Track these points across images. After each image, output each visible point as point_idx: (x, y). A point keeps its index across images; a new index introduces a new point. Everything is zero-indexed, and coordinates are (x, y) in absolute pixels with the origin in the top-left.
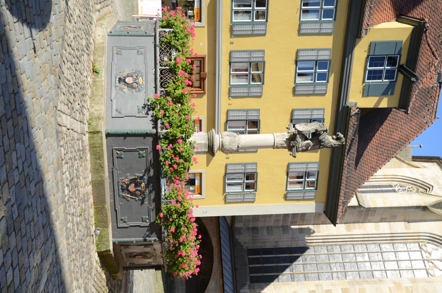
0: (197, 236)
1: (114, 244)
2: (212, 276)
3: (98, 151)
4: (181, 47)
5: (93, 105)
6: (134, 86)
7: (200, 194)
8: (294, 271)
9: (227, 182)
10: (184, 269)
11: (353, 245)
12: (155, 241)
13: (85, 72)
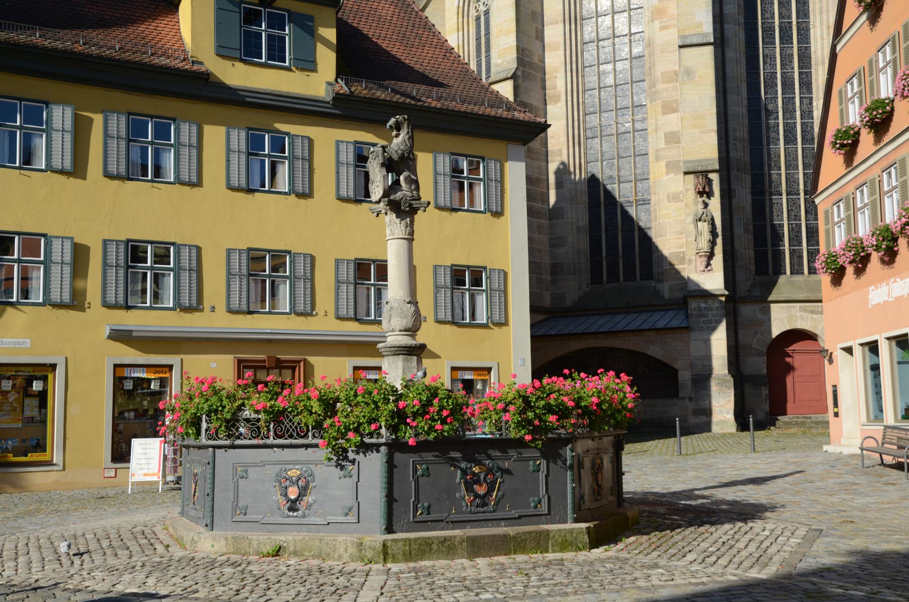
0: (565, 377)
1: (576, 521)
2: (639, 350)
3: (417, 546)
4: (235, 401)
5: (336, 556)
6: (304, 485)
7: (489, 370)
8: (631, 199)
9: (468, 321)
10: (622, 400)
11: (584, 91)
12: (572, 451)
13: (280, 567)
